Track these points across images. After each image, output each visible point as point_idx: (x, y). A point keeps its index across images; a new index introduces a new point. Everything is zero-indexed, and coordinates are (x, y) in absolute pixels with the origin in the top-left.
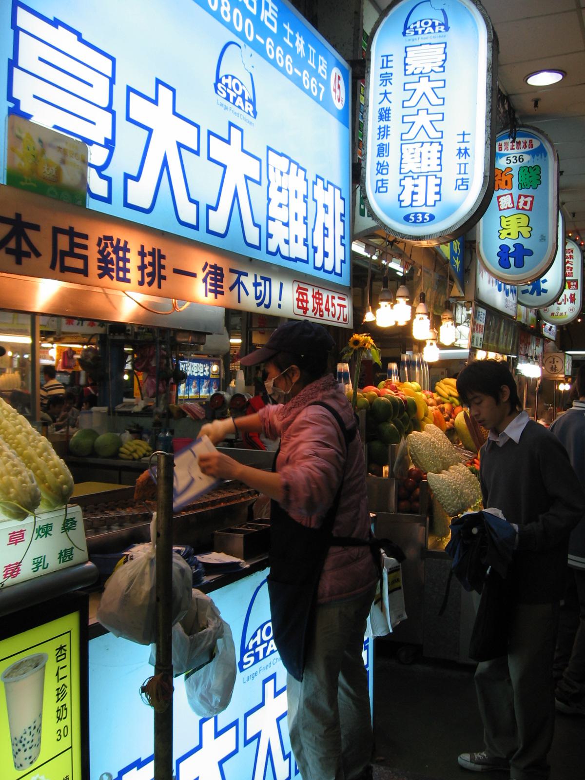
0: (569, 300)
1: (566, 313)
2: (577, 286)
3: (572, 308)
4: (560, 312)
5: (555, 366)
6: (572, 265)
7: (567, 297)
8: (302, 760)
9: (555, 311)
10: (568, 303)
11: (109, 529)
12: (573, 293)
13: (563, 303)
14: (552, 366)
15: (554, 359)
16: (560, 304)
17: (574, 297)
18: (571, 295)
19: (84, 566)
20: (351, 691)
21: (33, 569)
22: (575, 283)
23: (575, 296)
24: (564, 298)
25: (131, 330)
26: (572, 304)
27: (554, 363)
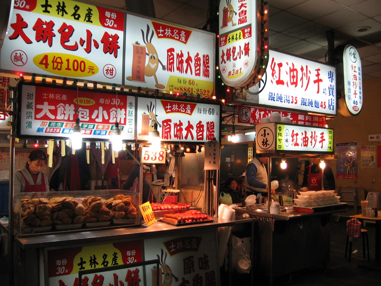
0: (244, 52)
1: (241, 69)
2: (250, 33)
3: (246, 62)
4: (236, 69)
5: (266, 139)
6: (246, 7)
7: (241, 49)
8: (109, 158)
9: (231, 70)
10: (243, 56)
11: (97, 209)
12: (247, 43)
13: (238, 57)
14: (264, 139)
15: (265, 130)
16: (235, 59)
17: (248, 47)
18: (245, 45)
19: (302, 214)
20: (108, 204)
21: (89, 67)
22: (249, 30)
23: (249, 46)
24: (239, 52)
25: (107, 186)
26: (247, 56)
27: (265, 136)
